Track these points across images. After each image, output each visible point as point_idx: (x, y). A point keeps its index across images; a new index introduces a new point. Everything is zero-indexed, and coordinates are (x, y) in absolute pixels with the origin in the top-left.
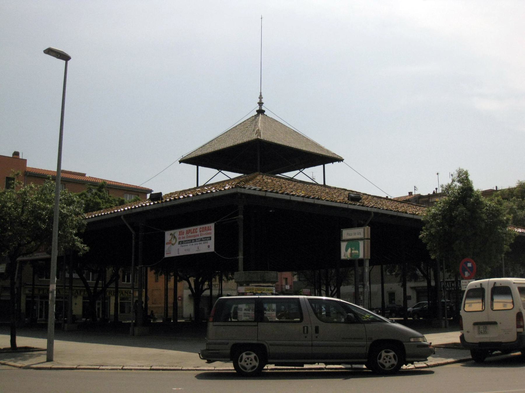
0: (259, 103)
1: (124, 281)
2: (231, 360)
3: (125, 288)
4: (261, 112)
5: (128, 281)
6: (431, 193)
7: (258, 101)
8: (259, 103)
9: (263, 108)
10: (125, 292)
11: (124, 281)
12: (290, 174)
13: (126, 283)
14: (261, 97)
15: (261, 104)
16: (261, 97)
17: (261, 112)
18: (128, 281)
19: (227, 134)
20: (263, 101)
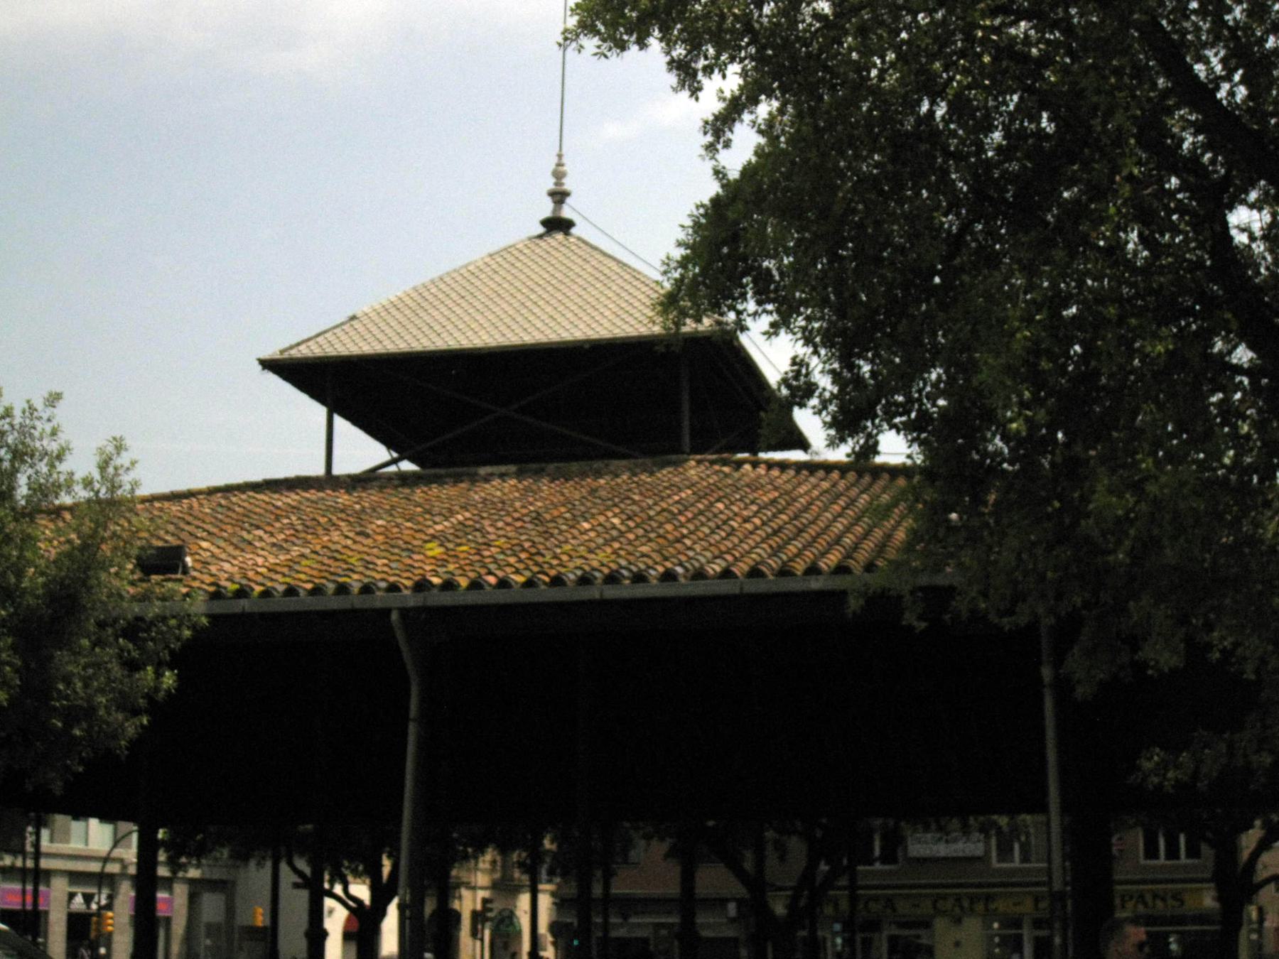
0: (552, 194)
1: (1156, 857)
2: (1237, 247)
3: (1153, 882)
4: (557, 225)
5: (1172, 853)
6: (893, 432)
7: (550, 184)
8: (552, 194)
9: (566, 213)
10: (1155, 896)
11: (1156, 857)
12: (995, 817)
13: (1162, 860)
14: (559, 175)
15: (559, 196)
16: (559, 175)
17: (557, 225)
18: (1172, 853)
19: (421, 300)
20: (568, 184)
